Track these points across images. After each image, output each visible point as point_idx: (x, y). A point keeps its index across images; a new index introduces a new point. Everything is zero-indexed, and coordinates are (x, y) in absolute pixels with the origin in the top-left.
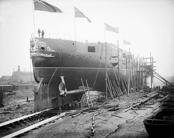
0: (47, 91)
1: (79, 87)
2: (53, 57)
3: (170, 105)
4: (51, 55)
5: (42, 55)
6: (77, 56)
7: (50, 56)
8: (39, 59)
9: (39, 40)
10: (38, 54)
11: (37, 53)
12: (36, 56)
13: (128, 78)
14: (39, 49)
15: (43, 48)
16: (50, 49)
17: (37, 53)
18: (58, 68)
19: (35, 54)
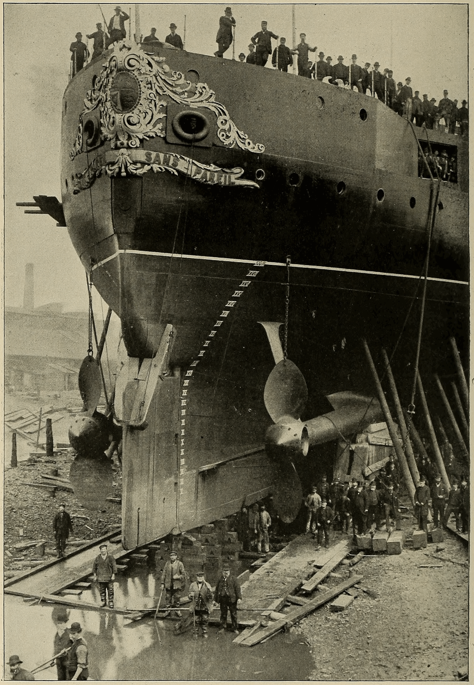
0: (180, 418)
1: (331, 396)
2: (248, 187)
3: (82, 544)
4: (239, 171)
5: (186, 165)
6: (381, 194)
7: (235, 177)
8: (170, 197)
9: (167, 68)
10: (157, 161)
11: (154, 155)
12: (147, 168)
13: (152, 351)
14: (164, 129)
15: (192, 122)
16: (233, 135)
17: (154, 155)
18: (262, 263)
19: (141, 155)
